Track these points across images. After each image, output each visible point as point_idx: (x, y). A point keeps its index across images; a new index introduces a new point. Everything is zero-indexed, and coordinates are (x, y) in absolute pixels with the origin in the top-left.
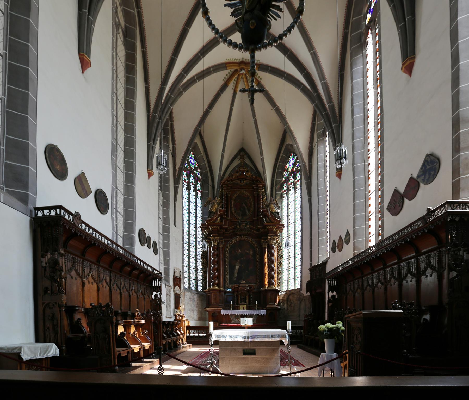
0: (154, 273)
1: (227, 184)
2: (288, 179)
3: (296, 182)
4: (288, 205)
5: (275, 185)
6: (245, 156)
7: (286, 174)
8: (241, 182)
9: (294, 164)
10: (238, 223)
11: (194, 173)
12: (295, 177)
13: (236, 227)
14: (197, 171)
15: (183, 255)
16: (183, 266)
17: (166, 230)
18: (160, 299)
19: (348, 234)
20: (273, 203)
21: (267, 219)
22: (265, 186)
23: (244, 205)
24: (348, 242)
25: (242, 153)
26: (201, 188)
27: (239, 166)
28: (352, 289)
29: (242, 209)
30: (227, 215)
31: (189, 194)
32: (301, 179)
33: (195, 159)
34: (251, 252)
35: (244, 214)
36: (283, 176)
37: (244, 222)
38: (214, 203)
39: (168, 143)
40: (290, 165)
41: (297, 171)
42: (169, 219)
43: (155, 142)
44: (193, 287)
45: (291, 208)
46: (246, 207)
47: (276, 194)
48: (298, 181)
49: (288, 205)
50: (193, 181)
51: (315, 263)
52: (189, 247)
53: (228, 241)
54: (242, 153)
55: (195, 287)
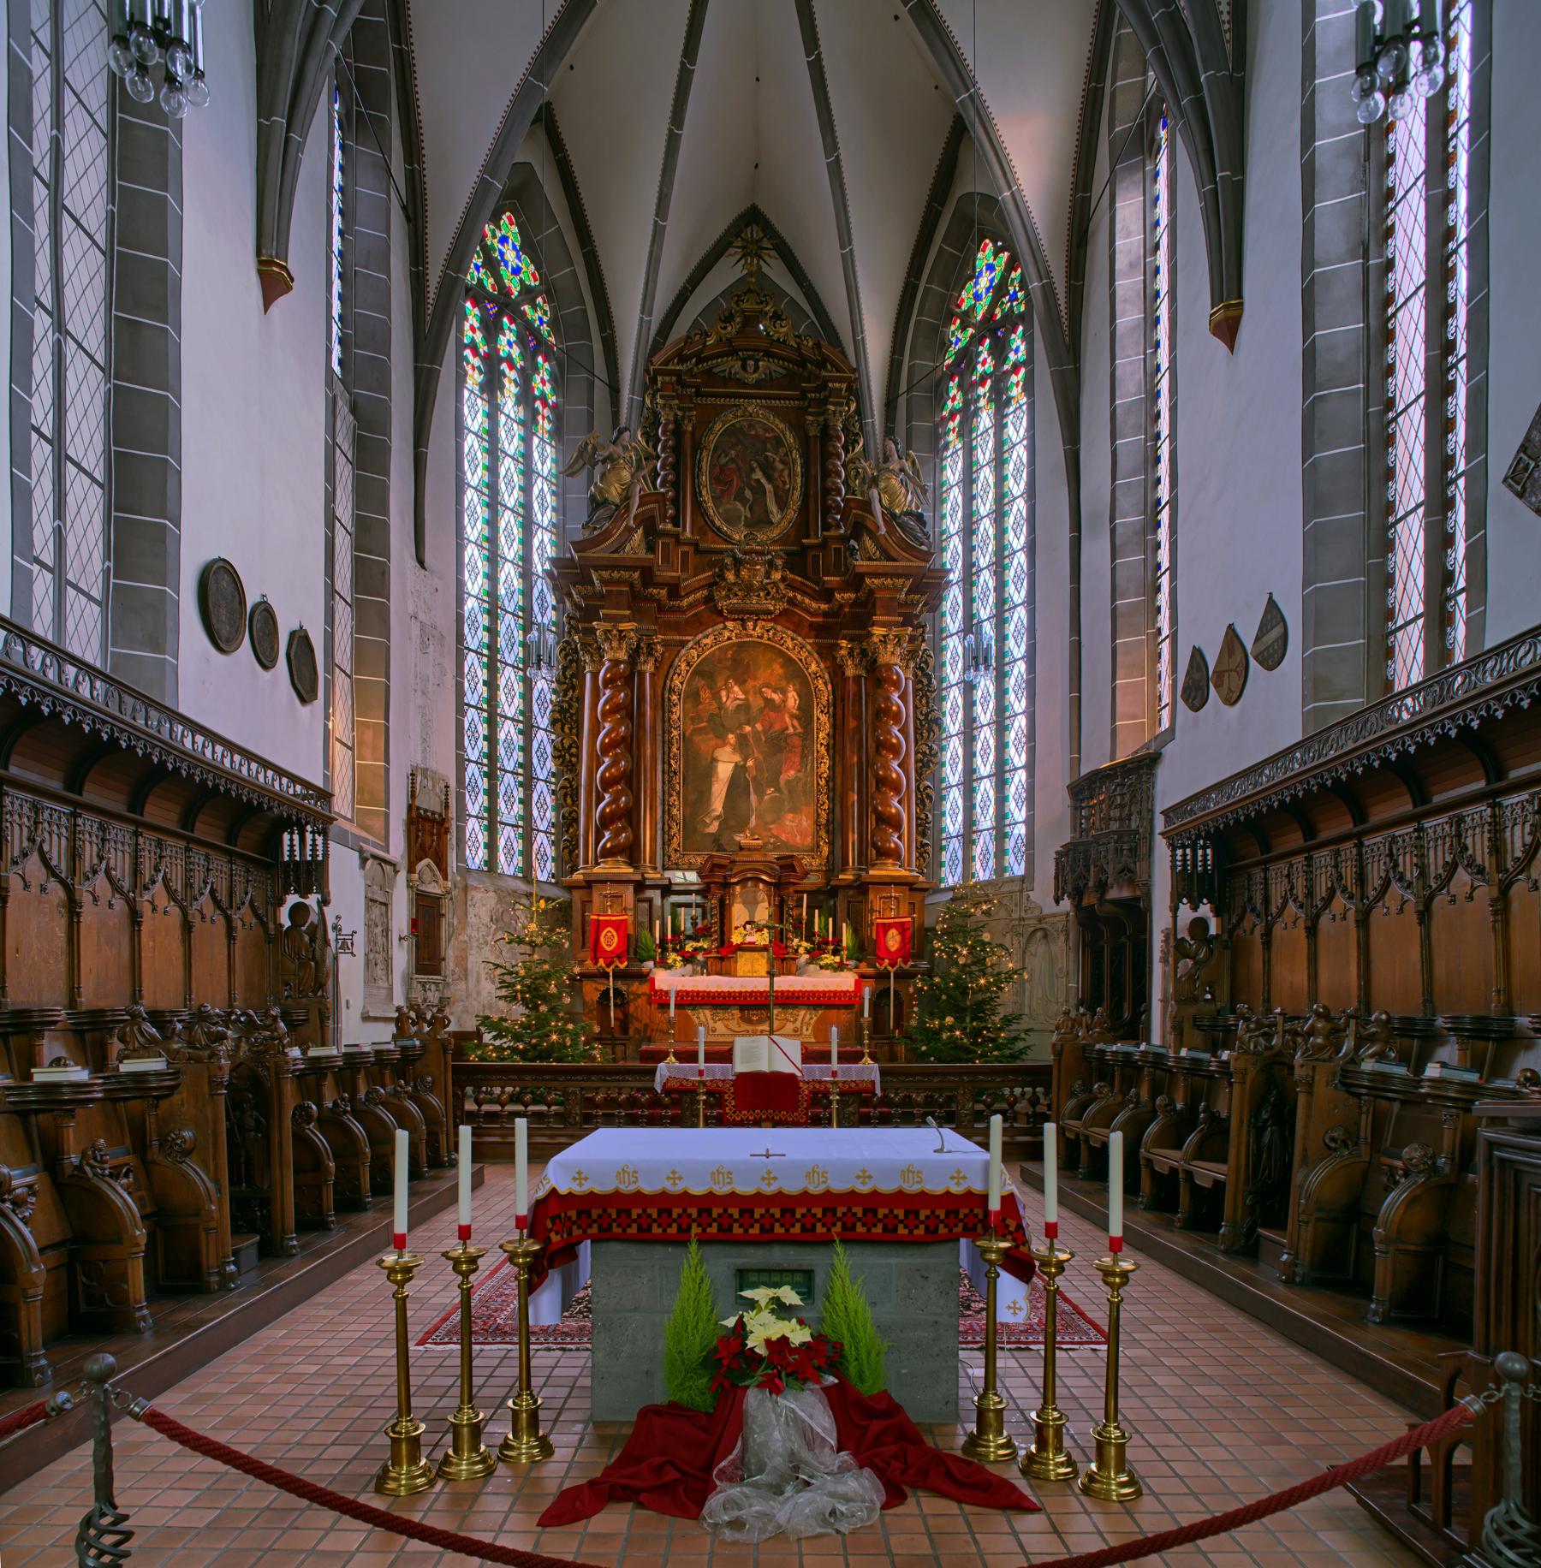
0: (281, 799)
1: (678, 374)
2: (967, 357)
3: (1007, 374)
4: (968, 480)
5: (903, 387)
6: (766, 244)
7: (959, 337)
8: (744, 368)
9: (999, 290)
10: (728, 561)
11: (517, 316)
12: (1000, 350)
13: (722, 577)
14: (535, 307)
15: (461, 708)
16: (461, 763)
17: (371, 578)
18: (318, 932)
19: (1273, 612)
20: (895, 466)
21: (868, 542)
22: (855, 390)
23: (758, 475)
24: (1272, 658)
25: (753, 230)
26: (554, 390)
27: (737, 292)
28: (1300, 891)
29: (748, 494)
30: (676, 521)
31: (493, 414)
32: (1029, 361)
33: (528, 247)
34: (793, 699)
35: (760, 520)
36: (944, 345)
37: (761, 553)
38: (610, 458)
39: (384, 148)
40: (977, 297)
41: (1011, 321)
42: (385, 527)
43: (298, 120)
44: (509, 865)
45: (983, 491)
46: (768, 487)
47: (909, 431)
48: (1016, 368)
49: (968, 480)
50: (515, 352)
51: (1096, 759)
52: (492, 667)
53: (683, 644)
54: (754, 232)
55: (518, 861)
